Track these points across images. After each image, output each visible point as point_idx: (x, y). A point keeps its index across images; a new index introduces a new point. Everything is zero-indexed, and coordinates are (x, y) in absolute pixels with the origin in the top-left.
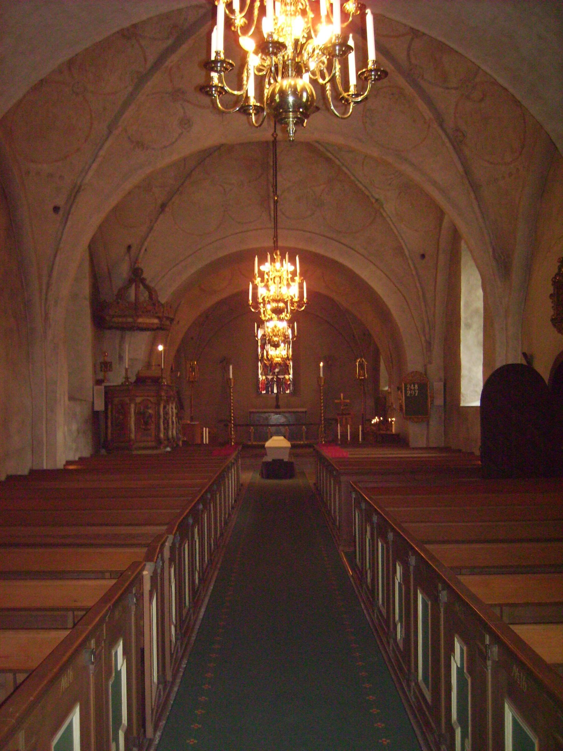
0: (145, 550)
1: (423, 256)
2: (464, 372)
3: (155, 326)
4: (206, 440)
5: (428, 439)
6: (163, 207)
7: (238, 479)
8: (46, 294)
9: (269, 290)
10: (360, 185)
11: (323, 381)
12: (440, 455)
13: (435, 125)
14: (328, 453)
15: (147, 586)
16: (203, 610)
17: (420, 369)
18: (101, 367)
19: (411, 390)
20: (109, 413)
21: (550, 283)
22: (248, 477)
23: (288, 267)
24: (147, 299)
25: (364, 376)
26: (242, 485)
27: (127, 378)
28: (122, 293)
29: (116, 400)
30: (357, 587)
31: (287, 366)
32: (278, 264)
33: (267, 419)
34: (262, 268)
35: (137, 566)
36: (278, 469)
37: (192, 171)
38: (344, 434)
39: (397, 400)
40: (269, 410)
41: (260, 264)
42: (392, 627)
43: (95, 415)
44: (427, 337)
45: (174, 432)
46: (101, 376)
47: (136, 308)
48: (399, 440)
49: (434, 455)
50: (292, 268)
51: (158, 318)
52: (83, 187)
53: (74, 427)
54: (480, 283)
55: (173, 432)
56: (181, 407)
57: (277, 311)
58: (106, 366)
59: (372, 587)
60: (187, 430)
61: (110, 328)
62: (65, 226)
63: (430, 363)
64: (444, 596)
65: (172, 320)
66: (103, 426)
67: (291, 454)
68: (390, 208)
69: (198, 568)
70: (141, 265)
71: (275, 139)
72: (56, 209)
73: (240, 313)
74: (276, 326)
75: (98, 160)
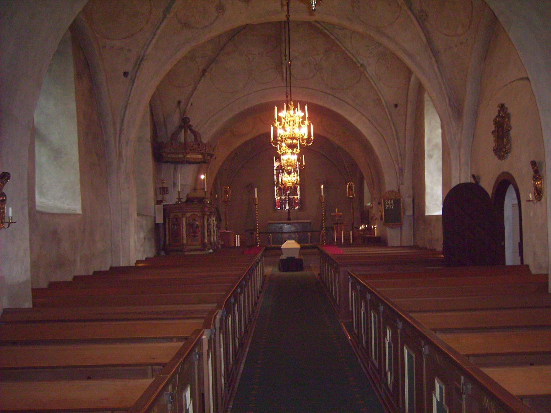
0: (202, 321)
1: (396, 106)
2: (428, 190)
3: (200, 160)
4: (238, 244)
5: (401, 240)
6: (204, 71)
7: (263, 271)
8: (120, 136)
9: (285, 131)
10: (349, 54)
11: (324, 198)
12: (409, 251)
13: (405, 8)
14: (330, 251)
15: (205, 347)
16: (242, 366)
17: (395, 189)
18: (160, 191)
19: (388, 204)
20: (167, 226)
21: (492, 123)
22: (269, 270)
23: (299, 113)
24: (193, 140)
25: (353, 195)
26: (266, 276)
27: (179, 199)
28: (174, 136)
29: (172, 216)
30: (355, 348)
31: (295, 188)
32: (292, 112)
33: (281, 228)
34: (280, 114)
35: (198, 332)
36: (291, 264)
37: (224, 45)
38: (339, 238)
39: (377, 212)
40: (283, 222)
41: (279, 111)
42: (383, 376)
43: (157, 225)
44: (400, 165)
45: (215, 239)
46: (160, 199)
47: (185, 146)
48: (380, 241)
49: (406, 251)
50: (302, 114)
51: (202, 154)
52: (145, 58)
53: (142, 235)
54: (439, 124)
55: (214, 238)
56: (219, 219)
57: (291, 146)
58: (164, 190)
59: (366, 346)
60: (224, 236)
61: (167, 162)
62: (133, 85)
63: (403, 184)
64: (426, 350)
65: (212, 156)
66: (162, 235)
67: (300, 253)
68: (371, 70)
69: (238, 336)
70: (188, 116)
71: (288, 19)
72: (126, 74)
73: (264, 148)
74: (289, 157)
75: (157, 36)
